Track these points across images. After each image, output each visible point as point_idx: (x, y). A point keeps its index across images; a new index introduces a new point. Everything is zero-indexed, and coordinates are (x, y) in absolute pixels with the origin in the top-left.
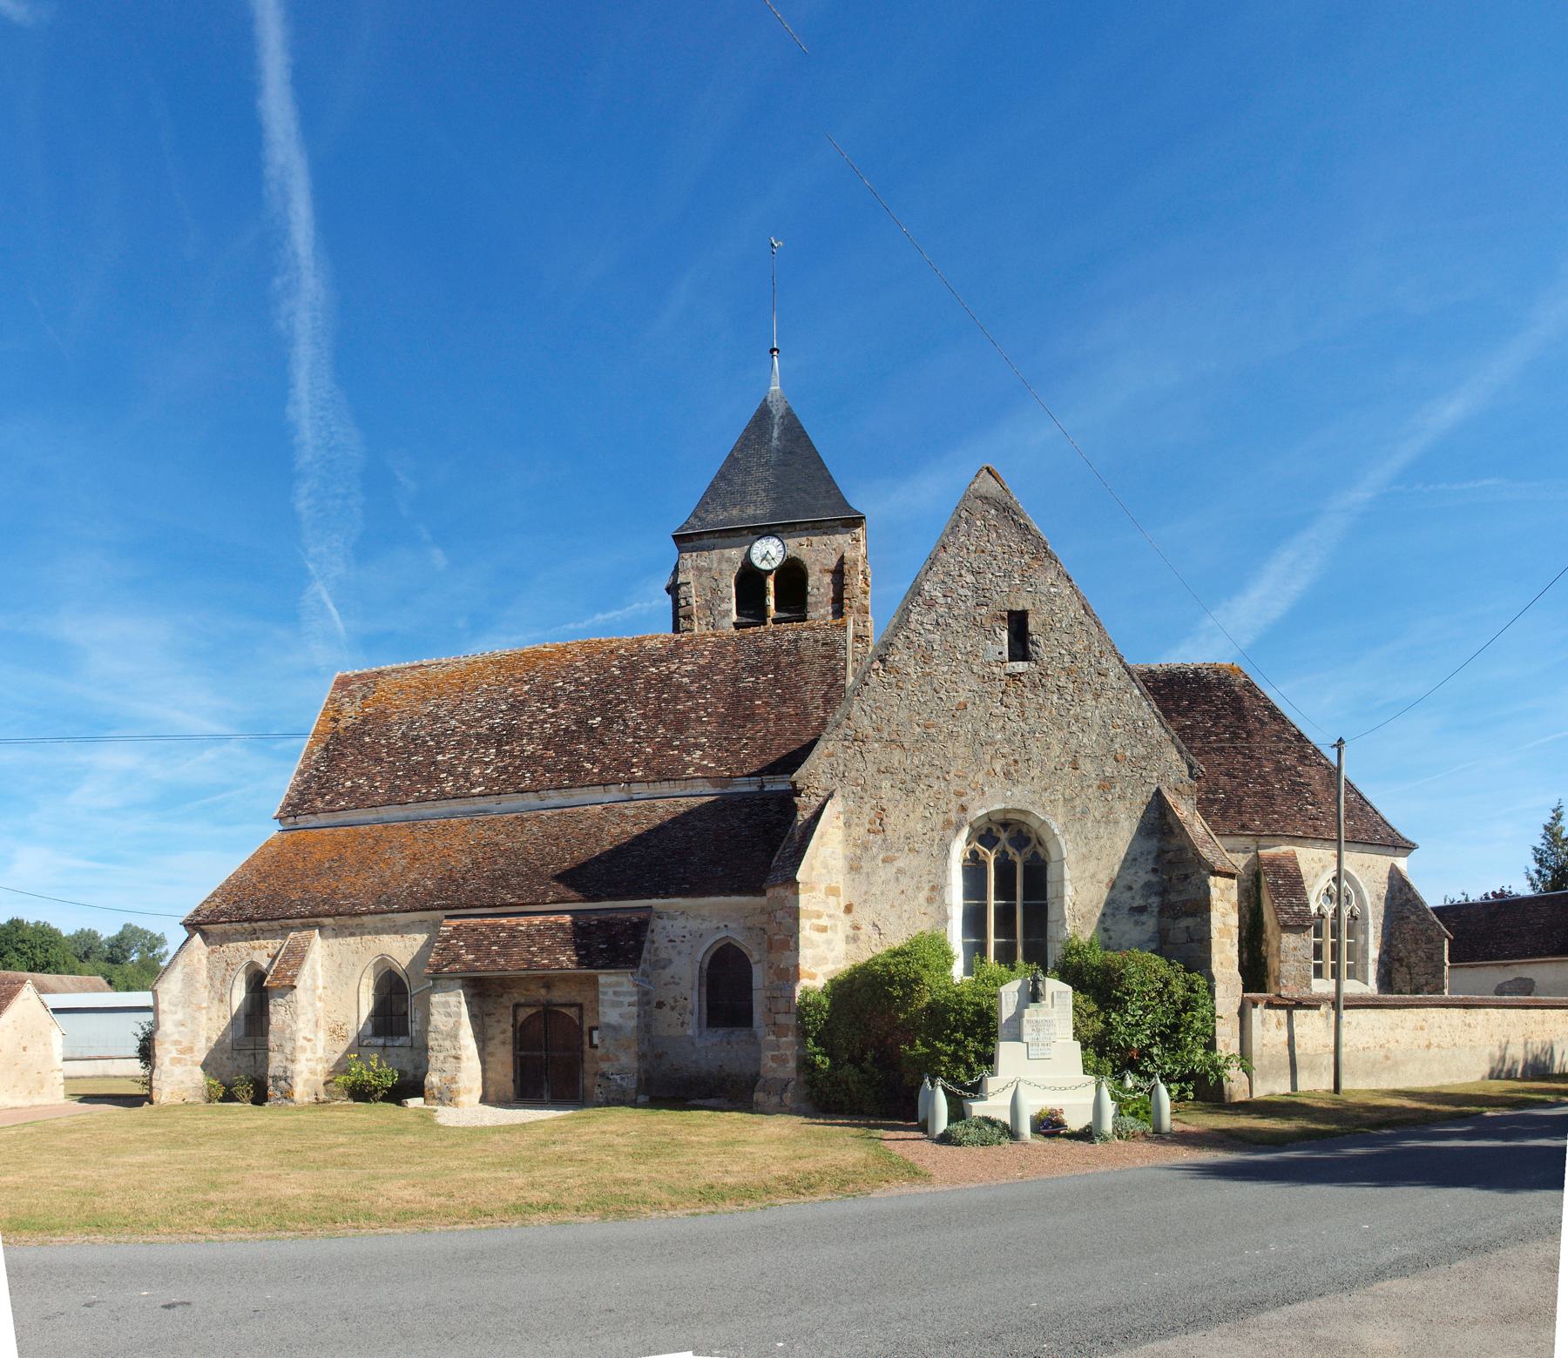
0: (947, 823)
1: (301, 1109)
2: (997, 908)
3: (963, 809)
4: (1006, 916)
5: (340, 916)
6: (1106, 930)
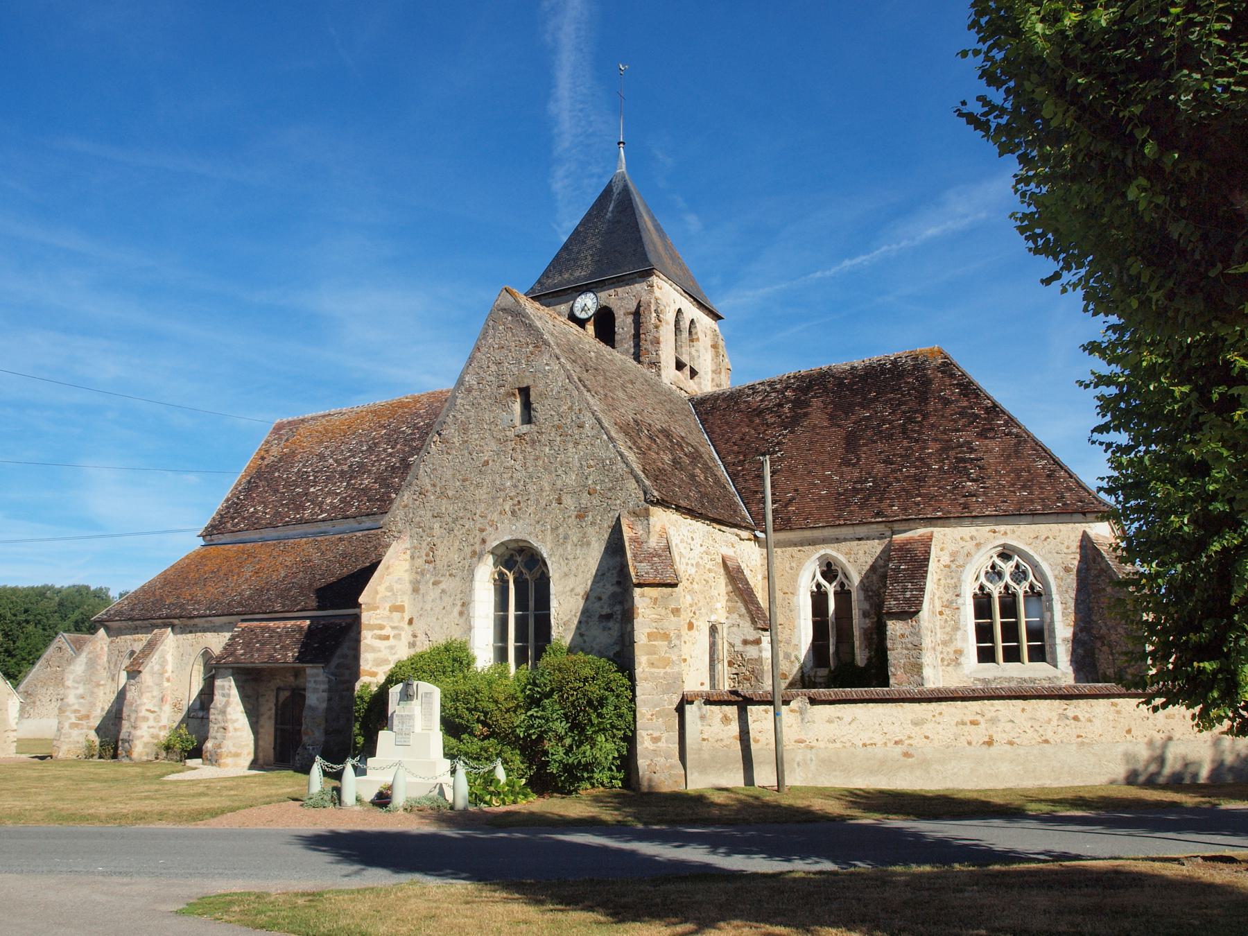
0: (474, 553)
1: (136, 764)
3: (484, 541)
4: (521, 623)
6: (581, 635)
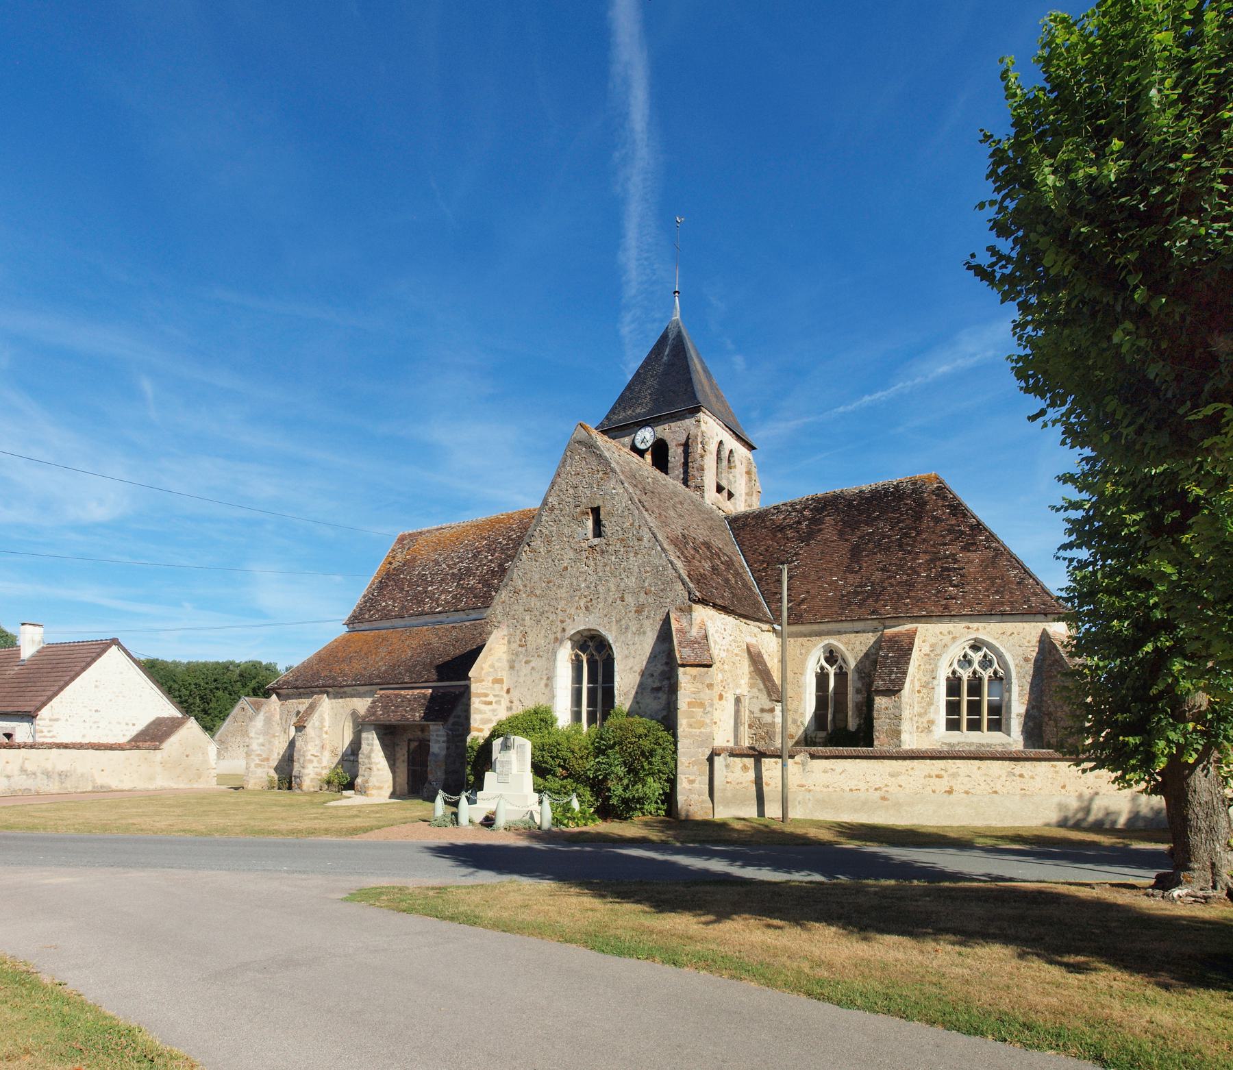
0: (556, 639)
2: (589, 689)
3: (564, 630)
4: (592, 692)
5: (336, 689)
